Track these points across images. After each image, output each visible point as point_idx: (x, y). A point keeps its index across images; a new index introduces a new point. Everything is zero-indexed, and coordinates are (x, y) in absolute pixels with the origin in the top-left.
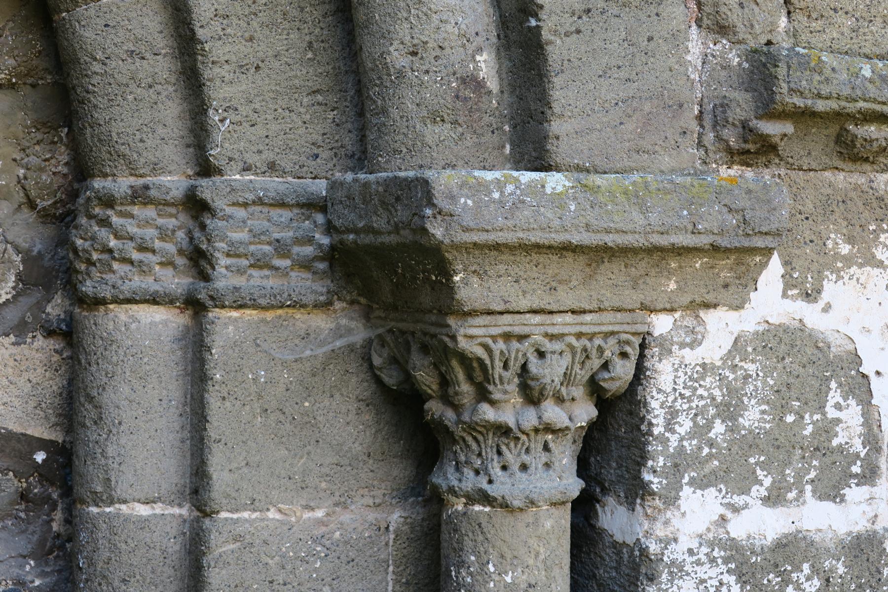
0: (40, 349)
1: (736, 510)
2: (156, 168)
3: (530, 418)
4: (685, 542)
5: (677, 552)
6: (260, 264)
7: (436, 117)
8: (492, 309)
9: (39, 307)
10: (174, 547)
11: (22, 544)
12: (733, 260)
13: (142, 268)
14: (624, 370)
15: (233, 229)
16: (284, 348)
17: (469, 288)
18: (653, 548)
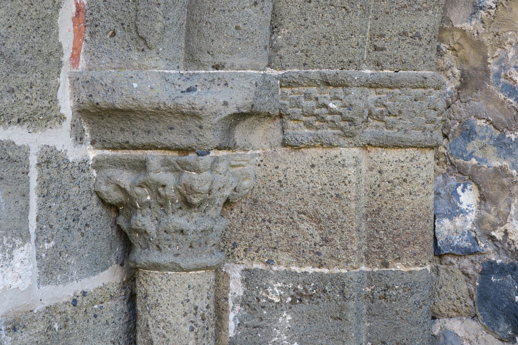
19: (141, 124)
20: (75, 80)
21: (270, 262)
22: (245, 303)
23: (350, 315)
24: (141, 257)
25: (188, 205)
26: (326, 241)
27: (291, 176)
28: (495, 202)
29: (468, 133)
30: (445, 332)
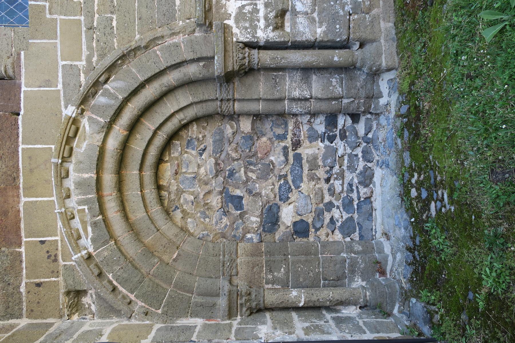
0: (241, 118)
2: (217, 105)
3: (247, 58)
4: (264, 35)
5: (265, 37)
6: (229, 92)
7: (209, 71)
8: (233, 65)
9: (236, 118)
10: (265, 102)
11: (266, 120)
12: (226, 29)
13: (230, 107)
14: (241, 45)
15: (224, 96)
16: (239, 90)
17: (230, 69)
18: (265, 40)
19: (232, 305)
20: (222, 320)
21: (263, 278)
22: (273, 284)
24: (262, 306)
25: (250, 294)
26: (258, 265)
27: (244, 274)
28: (249, 230)
29: (235, 236)
30: (278, 240)
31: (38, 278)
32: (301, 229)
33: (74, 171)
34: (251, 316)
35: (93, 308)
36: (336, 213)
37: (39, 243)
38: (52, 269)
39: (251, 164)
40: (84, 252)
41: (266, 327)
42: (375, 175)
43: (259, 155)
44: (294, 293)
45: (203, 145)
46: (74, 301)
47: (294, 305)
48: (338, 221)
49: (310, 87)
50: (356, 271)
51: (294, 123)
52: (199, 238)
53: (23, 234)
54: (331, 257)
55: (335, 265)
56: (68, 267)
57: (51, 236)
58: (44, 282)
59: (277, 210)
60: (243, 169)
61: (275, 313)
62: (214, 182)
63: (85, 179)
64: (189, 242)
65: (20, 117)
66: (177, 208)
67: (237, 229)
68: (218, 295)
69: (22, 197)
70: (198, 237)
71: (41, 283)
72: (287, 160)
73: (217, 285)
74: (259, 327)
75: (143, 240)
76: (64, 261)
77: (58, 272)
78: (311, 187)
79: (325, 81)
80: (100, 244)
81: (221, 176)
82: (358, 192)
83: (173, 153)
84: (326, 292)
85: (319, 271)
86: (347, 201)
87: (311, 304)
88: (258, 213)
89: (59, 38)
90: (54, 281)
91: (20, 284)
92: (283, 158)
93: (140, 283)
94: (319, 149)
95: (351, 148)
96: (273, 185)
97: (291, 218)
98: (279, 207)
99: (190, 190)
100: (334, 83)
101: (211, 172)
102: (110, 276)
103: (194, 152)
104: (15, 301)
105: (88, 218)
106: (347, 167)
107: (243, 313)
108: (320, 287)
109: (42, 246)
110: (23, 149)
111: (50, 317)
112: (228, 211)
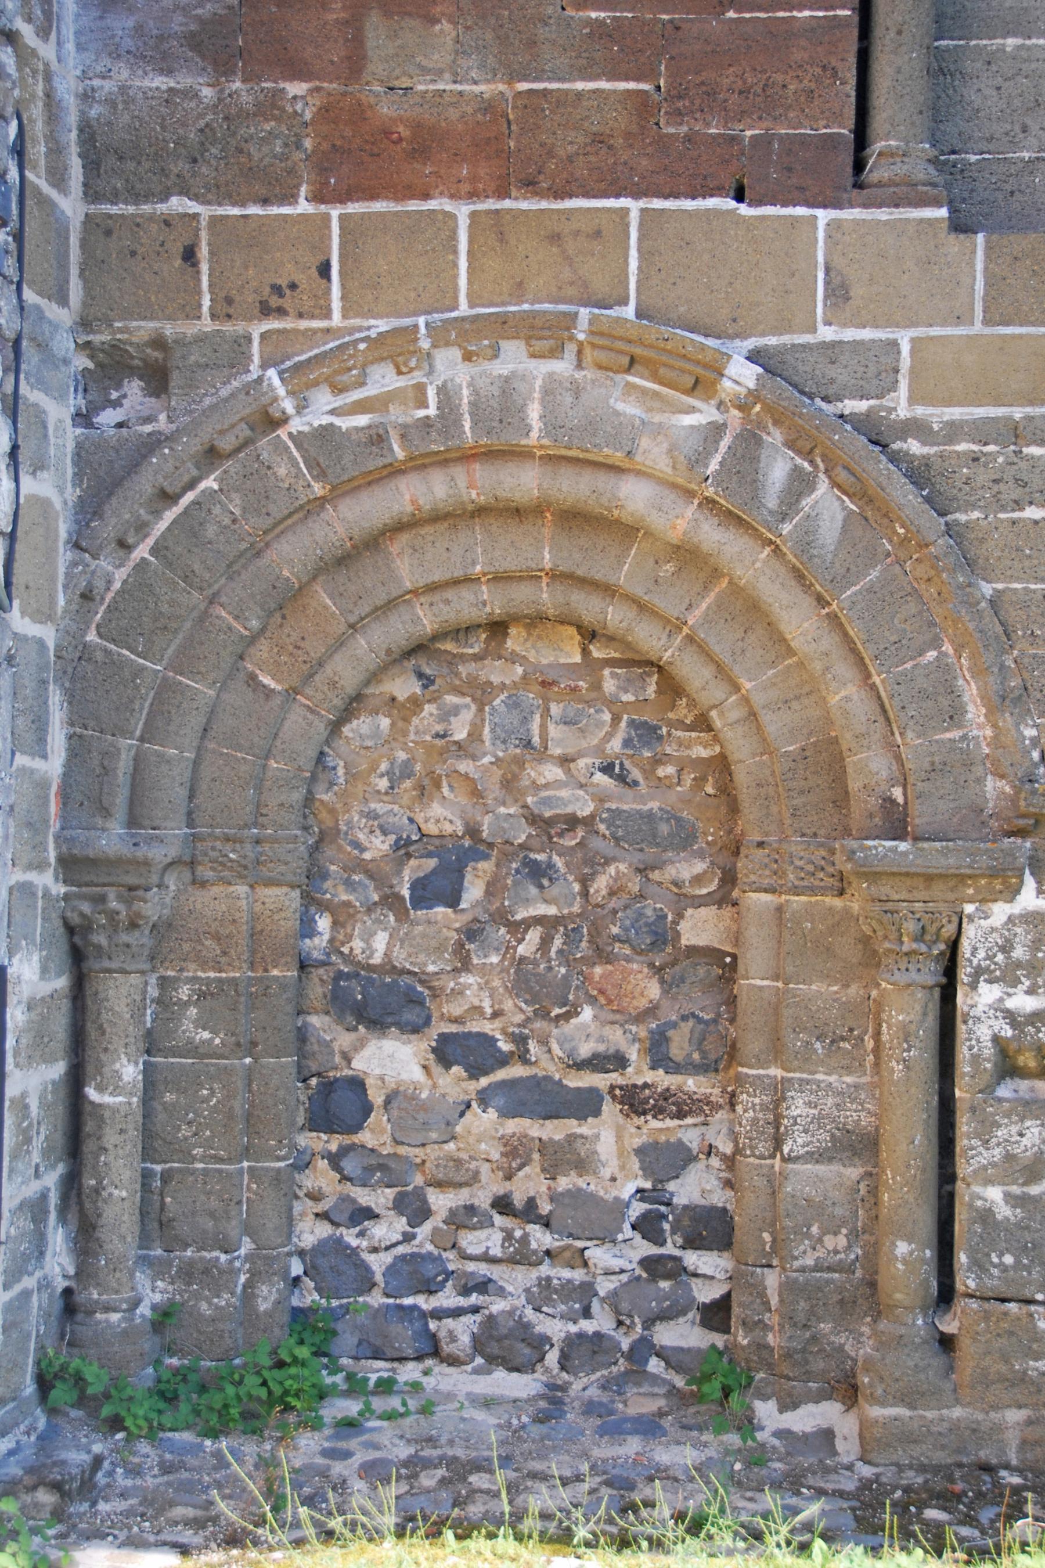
1: (1009, 995)
4: (981, 1007)
21: (181, 970)
23: (241, 1007)
24: (92, 964)
26: (225, 953)
27: (199, 906)
28: (343, 926)
31: (211, 253)
32: (339, 1103)
33: (551, 375)
34: (62, 930)
35: (108, 417)
36: (388, 1229)
37: (322, 258)
38: (238, 298)
39: (572, 938)
40: (288, 406)
41: (36, 978)
42: (515, 1375)
43: (598, 970)
44: (130, 1072)
45: (640, 778)
46: (132, 358)
47: (90, 1069)
48: (361, 1234)
49: (818, 1157)
50: (189, 1284)
51: (707, 1096)
52: (322, 753)
53: (353, 208)
54: (239, 1203)
55: (212, 1214)
56: (244, 349)
57: (343, 298)
58: (198, 272)
59: (407, 1023)
60: (552, 911)
61: (65, 1005)
62: (512, 811)
63: (522, 409)
64: (310, 725)
65: (732, 204)
66: (427, 681)
67: (349, 885)
68: (133, 822)
69: (472, 207)
70: (326, 749)
71: (195, 264)
72: (580, 1066)
73: (165, 818)
74: (36, 958)
75: (321, 579)
76: (263, 336)
77: (229, 316)
78: (483, 1146)
79: (839, 1211)
80: (313, 451)
81: (530, 836)
82: (457, 1313)
83: (613, 675)
84: (127, 1175)
85: (194, 1159)
86: (430, 1269)
87: (89, 1127)
88: (401, 957)
89: (988, 331)
90: (200, 306)
91: (195, 197)
92: (585, 1050)
93: (185, 578)
94: (613, 1179)
95: (615, 1293)
96: (496, 1015)
97: (377, 1071)
98: (416, 1030)
99: (487, 730)
100: (829, 1242)
101: (546, 802)
102: (210, 483)
103: (615, 745)
104: (141, 180)
105: (398, 415)
106: (548, 1279)
107: (76, 903)
108: (144, 1160)
109: (314, 270)
110: (625, 212)
111: (88, 289)
112: (409, 856)
